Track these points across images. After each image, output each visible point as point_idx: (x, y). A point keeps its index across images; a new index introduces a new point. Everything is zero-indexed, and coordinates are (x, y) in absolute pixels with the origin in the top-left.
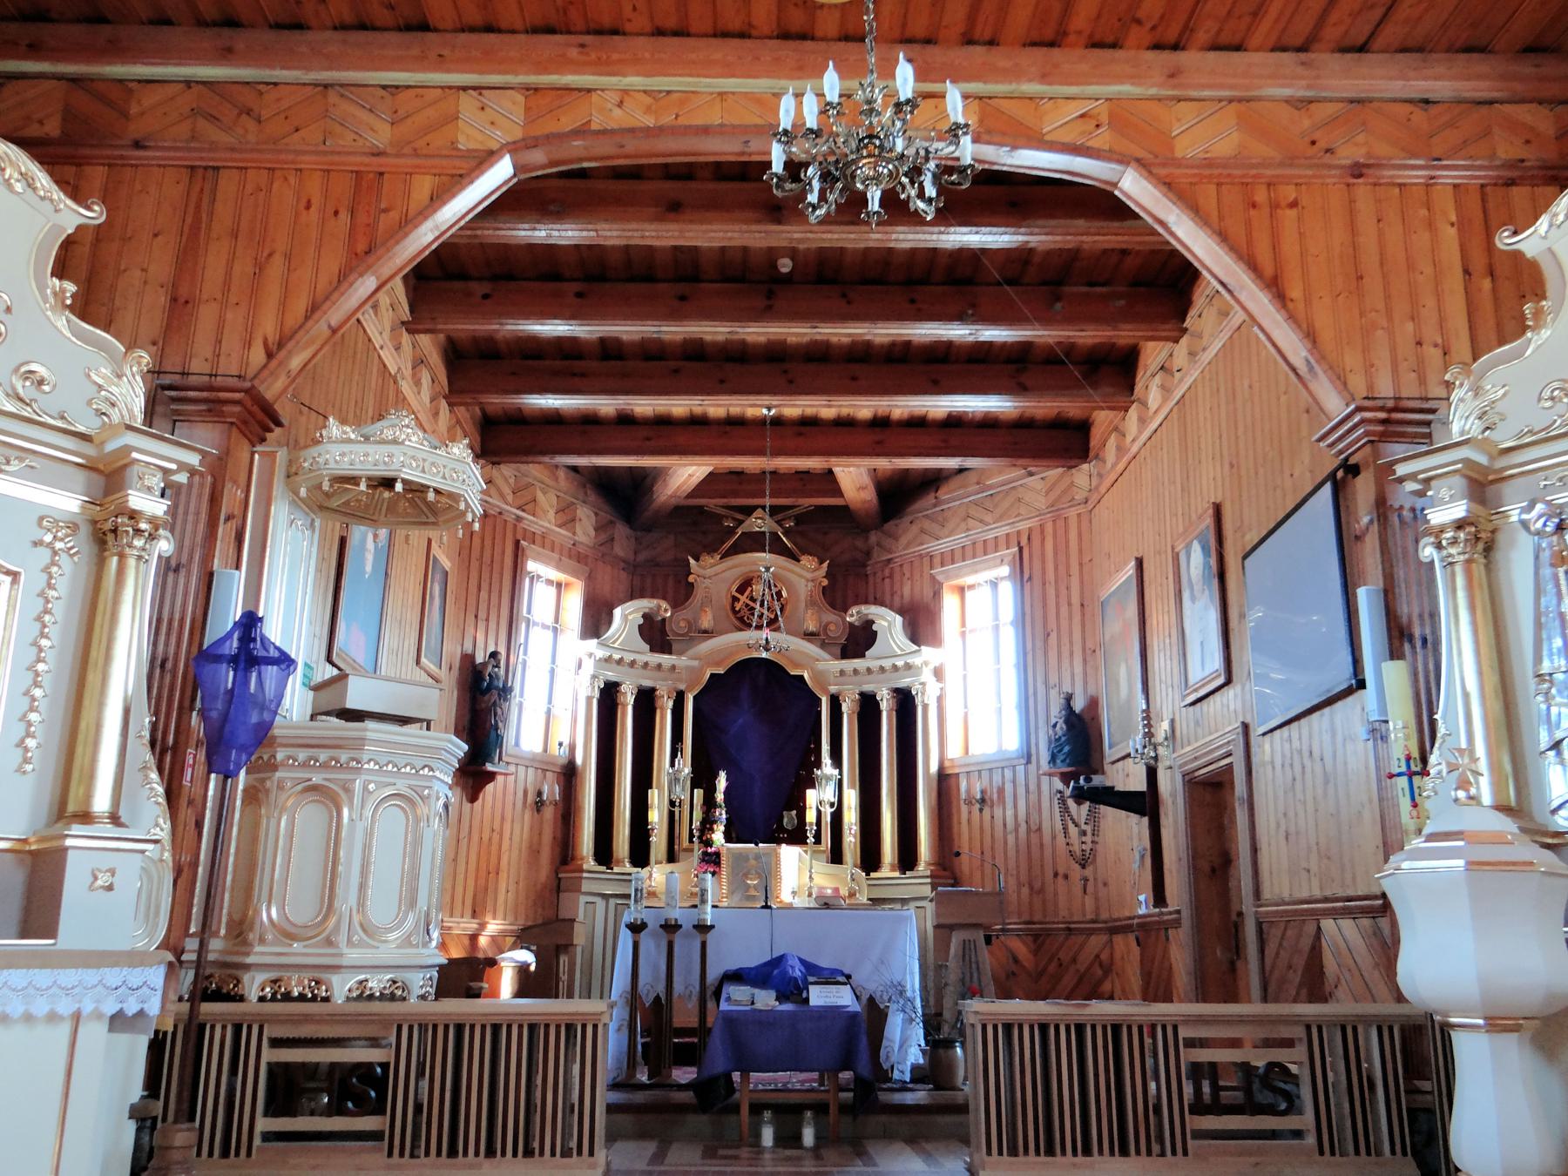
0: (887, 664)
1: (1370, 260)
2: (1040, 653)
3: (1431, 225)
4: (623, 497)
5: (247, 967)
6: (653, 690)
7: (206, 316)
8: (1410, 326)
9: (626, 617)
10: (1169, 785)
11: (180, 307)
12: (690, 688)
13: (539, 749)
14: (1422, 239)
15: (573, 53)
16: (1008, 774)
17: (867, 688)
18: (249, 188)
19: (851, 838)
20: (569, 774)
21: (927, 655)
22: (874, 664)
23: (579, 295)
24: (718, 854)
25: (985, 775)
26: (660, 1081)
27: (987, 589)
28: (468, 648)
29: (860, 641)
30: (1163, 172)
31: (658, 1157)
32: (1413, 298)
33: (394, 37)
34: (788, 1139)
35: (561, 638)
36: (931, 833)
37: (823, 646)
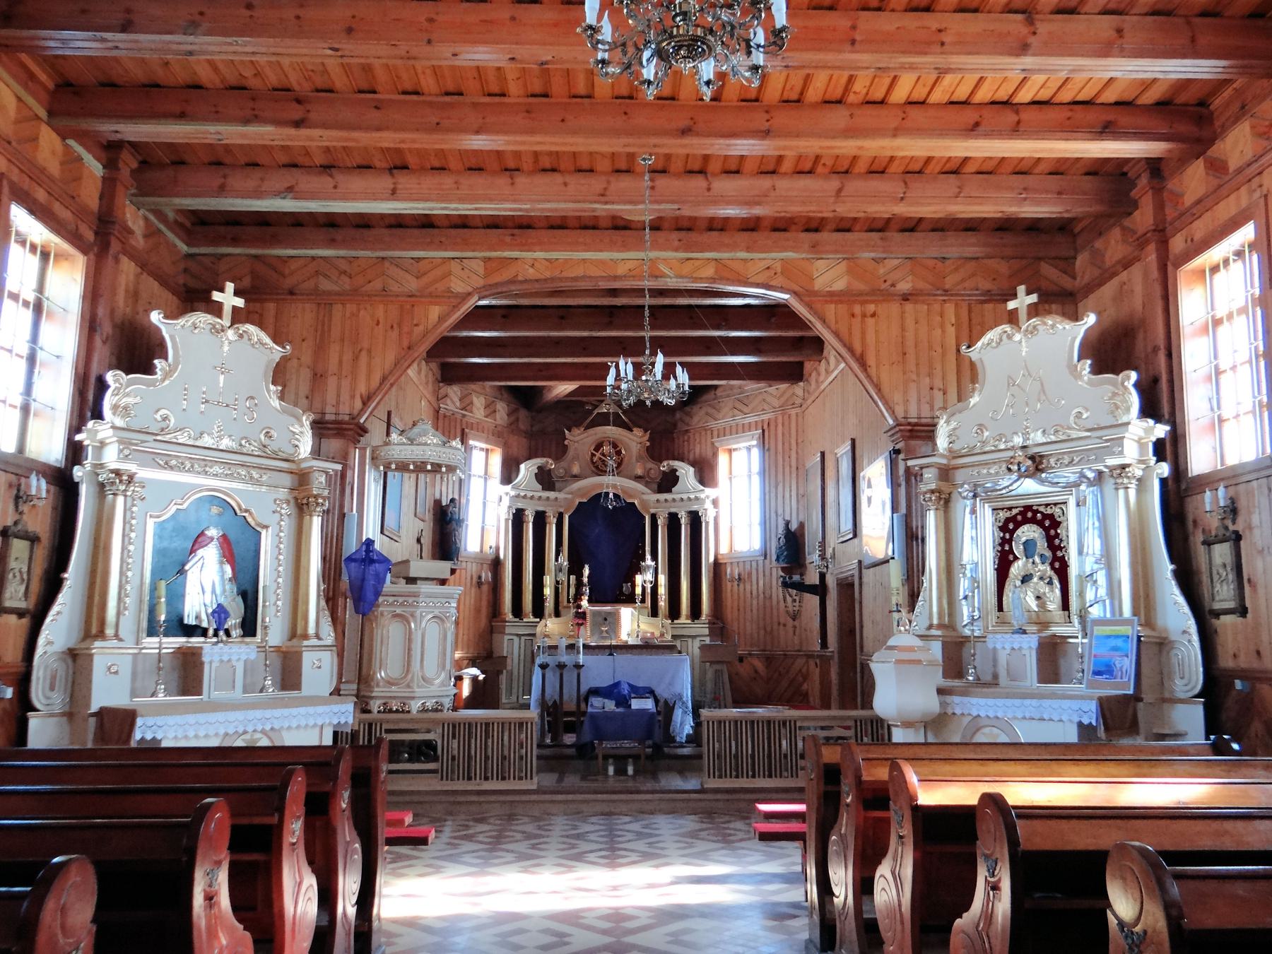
0: (685, 496)
1: (910, 343)
2: (773, 490)
3: (942, 326)
4: (525, 399)
5: (372, 698)
6: (544, 512)
7: (332, 382)
8: (927, 380)
9: (526, 470)
10: (831, 582)
11: (318, 377)
12: (567, 511)
13: (478, 550)
14: (938, 332)
15: (508, 239)
16: (754, 564)
17: (673, 510)
18: (348, 314)
19: (663, 604)
20: (496, 564)
21: (709, 492)
22: (677, 497)
23: (504, 316)
24: (584, 613)
25: (741, 565)
26: (557, 743)
27: (744, 452)
28: (437, 496)
29: (668, 482)
30: (807, 299)
31: (560, 780)
32: (931, 367)
33: (416, 232)
34: (621, 771)
35: (489, 482)
36: (709, 592)
37: (647, 485)
